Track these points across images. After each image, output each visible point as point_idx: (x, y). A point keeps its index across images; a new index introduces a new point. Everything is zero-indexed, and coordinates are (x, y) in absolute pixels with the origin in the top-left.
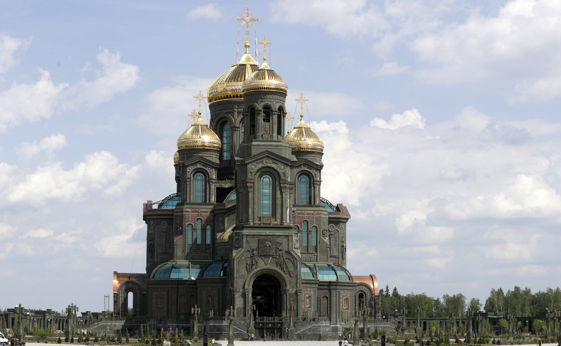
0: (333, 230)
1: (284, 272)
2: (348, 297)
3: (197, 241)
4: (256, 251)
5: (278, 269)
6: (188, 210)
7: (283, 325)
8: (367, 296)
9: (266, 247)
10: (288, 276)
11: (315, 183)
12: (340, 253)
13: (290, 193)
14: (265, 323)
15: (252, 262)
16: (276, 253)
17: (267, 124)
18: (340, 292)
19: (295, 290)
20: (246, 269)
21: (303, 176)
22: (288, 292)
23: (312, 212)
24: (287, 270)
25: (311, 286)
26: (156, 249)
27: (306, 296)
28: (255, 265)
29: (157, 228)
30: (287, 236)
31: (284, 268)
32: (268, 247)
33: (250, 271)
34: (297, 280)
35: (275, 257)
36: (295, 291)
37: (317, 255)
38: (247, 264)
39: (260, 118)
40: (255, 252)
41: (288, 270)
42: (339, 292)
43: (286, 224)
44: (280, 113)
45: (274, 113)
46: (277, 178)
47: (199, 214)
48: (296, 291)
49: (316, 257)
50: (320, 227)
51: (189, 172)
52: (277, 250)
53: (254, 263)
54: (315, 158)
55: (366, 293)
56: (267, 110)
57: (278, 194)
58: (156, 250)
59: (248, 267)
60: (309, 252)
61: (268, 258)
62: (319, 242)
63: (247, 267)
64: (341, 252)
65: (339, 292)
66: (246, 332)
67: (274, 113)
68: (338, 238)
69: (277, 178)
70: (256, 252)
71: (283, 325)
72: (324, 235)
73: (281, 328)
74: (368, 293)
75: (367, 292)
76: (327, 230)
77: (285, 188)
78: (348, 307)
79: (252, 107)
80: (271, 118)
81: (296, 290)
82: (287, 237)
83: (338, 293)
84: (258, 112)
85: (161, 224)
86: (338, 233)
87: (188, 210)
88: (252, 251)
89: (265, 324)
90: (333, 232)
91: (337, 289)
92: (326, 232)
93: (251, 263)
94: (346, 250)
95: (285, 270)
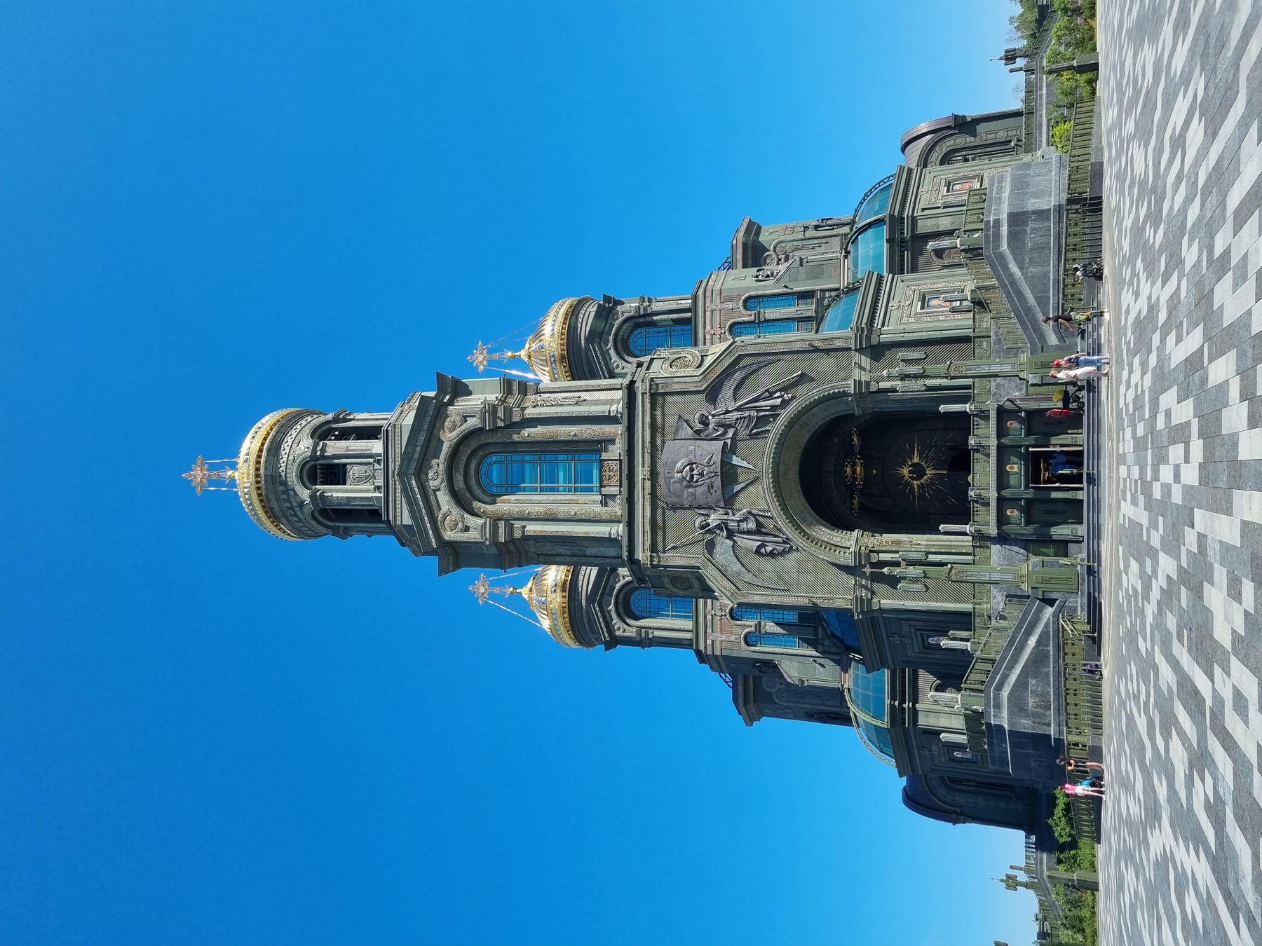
0: (774, 256)
1: (785, 403)
2: (943, 181)
3: (790, 621)
4: (708, 516)
5: (776, 428)
6: (709, 642)
7: (1009, 406)
8: (958, 147)
9: (692, 477)
10: (801, 390)
11: (642, 312)
12: (834, 232)
13: (537, 393)
14: (1003, 493)
15: (749, 532)
16: (713, 439)
17: (354, 472)
18: (921, 207)
19: (857, 357)
20: (780, 558)
21: (631, 345)
22: (868, 384)
23: (708, 314)
24: (778, 394)
25: (886, 296)
26: (831, 709)
27: (919, 311)
28: (760, 519)
29: (779, 702)
30: (654, 397)
31: (773, 408)
32: (692, 470)
33: (785, 543)
34: (817, 350)
35: (729, 441)
36: (863, 357)
37: (821, 291)
38: (758, 552)
39: (336, 493)
40: (714, 519)
41: (780, 390)
42: (923, 210)
43: (617, 408)
44: (336, 429)
45: (318, 453)
46: (484, 439)
47: (719, 613)
48: (860, 350)
49: (827, 294)
50: (748, 289)
51: (624, 631)
52: (703, 435)
53: (752, 525)
54: (587, 315)
55: (948, 149)
56: (319, 471)
57: (529, 436)
58: (836, 710)
59: (769, 549)
60: (814, 315)
61: (739, 470)
62: (786, 287)
63: (772, 554)
64: (833, 229)
65: (923, 210)
66: (1049, 611)
67: (318, 453)
68: (795, 243)
69: (484, 439)
70: (712, 516)
71: (1013, 407)
72: (768, 276)
73: (1028, 412)
74: (948, 144)
75: (944, 148)
76: (758, 271)
77: (509, 412)
78: (974, 177)
79: (316, 514)
80: (336, 461)
81: (856, 350)
82: (660, 400)
83: (927, 212)
84: (319, 501)
85: (770, 690)
86: (783, 244)
87: (709, 642)
88: (710, 531)
89: (1005, 493)
90: (780, 257)
91: (913, 218)
92: (761, 273)
93: (754, 537)
94: (827, 219)
95: (778, 401)
